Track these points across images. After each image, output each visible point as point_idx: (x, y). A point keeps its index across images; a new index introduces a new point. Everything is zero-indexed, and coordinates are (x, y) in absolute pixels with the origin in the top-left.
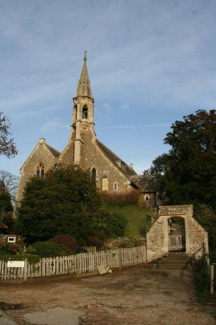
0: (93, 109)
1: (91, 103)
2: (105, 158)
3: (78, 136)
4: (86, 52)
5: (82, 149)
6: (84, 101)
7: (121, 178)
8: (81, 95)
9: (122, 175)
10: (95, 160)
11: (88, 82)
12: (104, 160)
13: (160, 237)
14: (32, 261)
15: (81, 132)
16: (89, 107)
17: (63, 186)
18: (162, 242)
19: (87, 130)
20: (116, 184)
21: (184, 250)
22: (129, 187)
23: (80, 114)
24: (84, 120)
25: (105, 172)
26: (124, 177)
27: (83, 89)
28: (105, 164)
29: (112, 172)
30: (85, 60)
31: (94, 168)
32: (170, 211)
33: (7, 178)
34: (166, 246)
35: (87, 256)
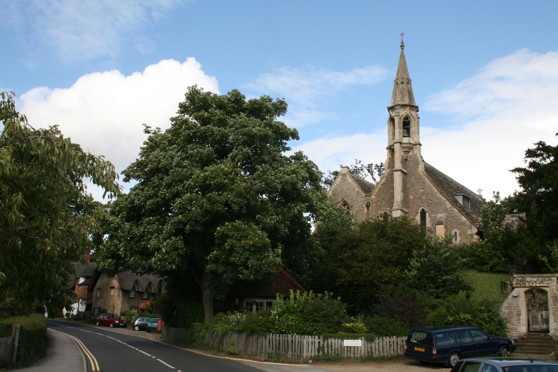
0: (418, 123)
2: (439, 195)
3: (398, 165)
4: (402, 35)
6: (403, 112)
8: (400, 103)
9: (465, 220)
10: (424, 197)
11: (409, 82)
12: (438, 198)
13: (515, 313)
14: (369, 340)
15: (402, 157)
16: (412, 119)
17: (387, 245)
18: (519, 320)
19: (411, 153)
20: (456, 233)
21: (547, 331)
22: (476, 237)
23: (398, 131)
24: (406, 140)
25: (439, 215)
26: (468, 223)
29: (450, 216)
30: (402, 46)
31: (423, 210)
32: (528, 282)
34: (523, 325)
35: (313, 340)
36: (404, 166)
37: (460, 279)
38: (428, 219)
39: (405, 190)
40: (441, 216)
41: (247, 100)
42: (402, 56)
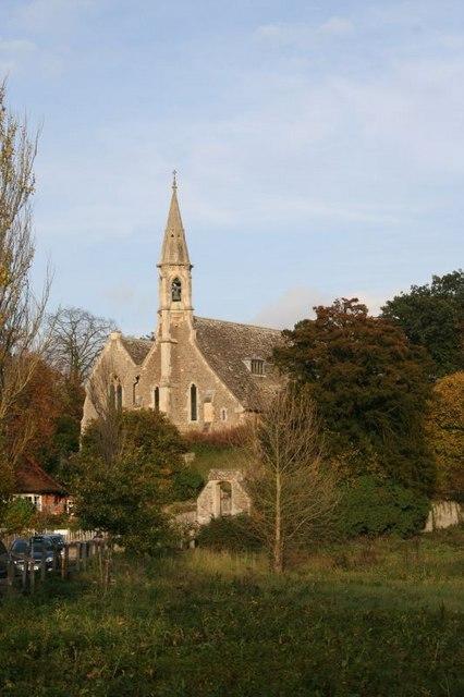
0: (190, 283)
1: (185, 272)
2: (209, 369)
4: (175, 172)
5: (174, 354)
6: (173, 273)
7: (230, 402)
12: (208, 373)
19: (181, 320)
27: (172, 251)
28: (208, 379)
30: (175, 188)
33: (83, 327)
36: (174, 336)
37: (271, 354)
38: (198, 396)
39: (174, 361)
40: (210, 392)
41: (374, 312)
42: (175, 200)
